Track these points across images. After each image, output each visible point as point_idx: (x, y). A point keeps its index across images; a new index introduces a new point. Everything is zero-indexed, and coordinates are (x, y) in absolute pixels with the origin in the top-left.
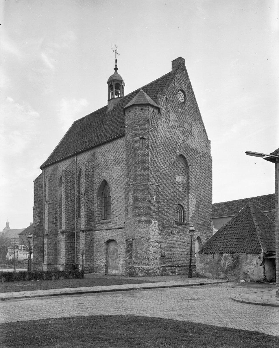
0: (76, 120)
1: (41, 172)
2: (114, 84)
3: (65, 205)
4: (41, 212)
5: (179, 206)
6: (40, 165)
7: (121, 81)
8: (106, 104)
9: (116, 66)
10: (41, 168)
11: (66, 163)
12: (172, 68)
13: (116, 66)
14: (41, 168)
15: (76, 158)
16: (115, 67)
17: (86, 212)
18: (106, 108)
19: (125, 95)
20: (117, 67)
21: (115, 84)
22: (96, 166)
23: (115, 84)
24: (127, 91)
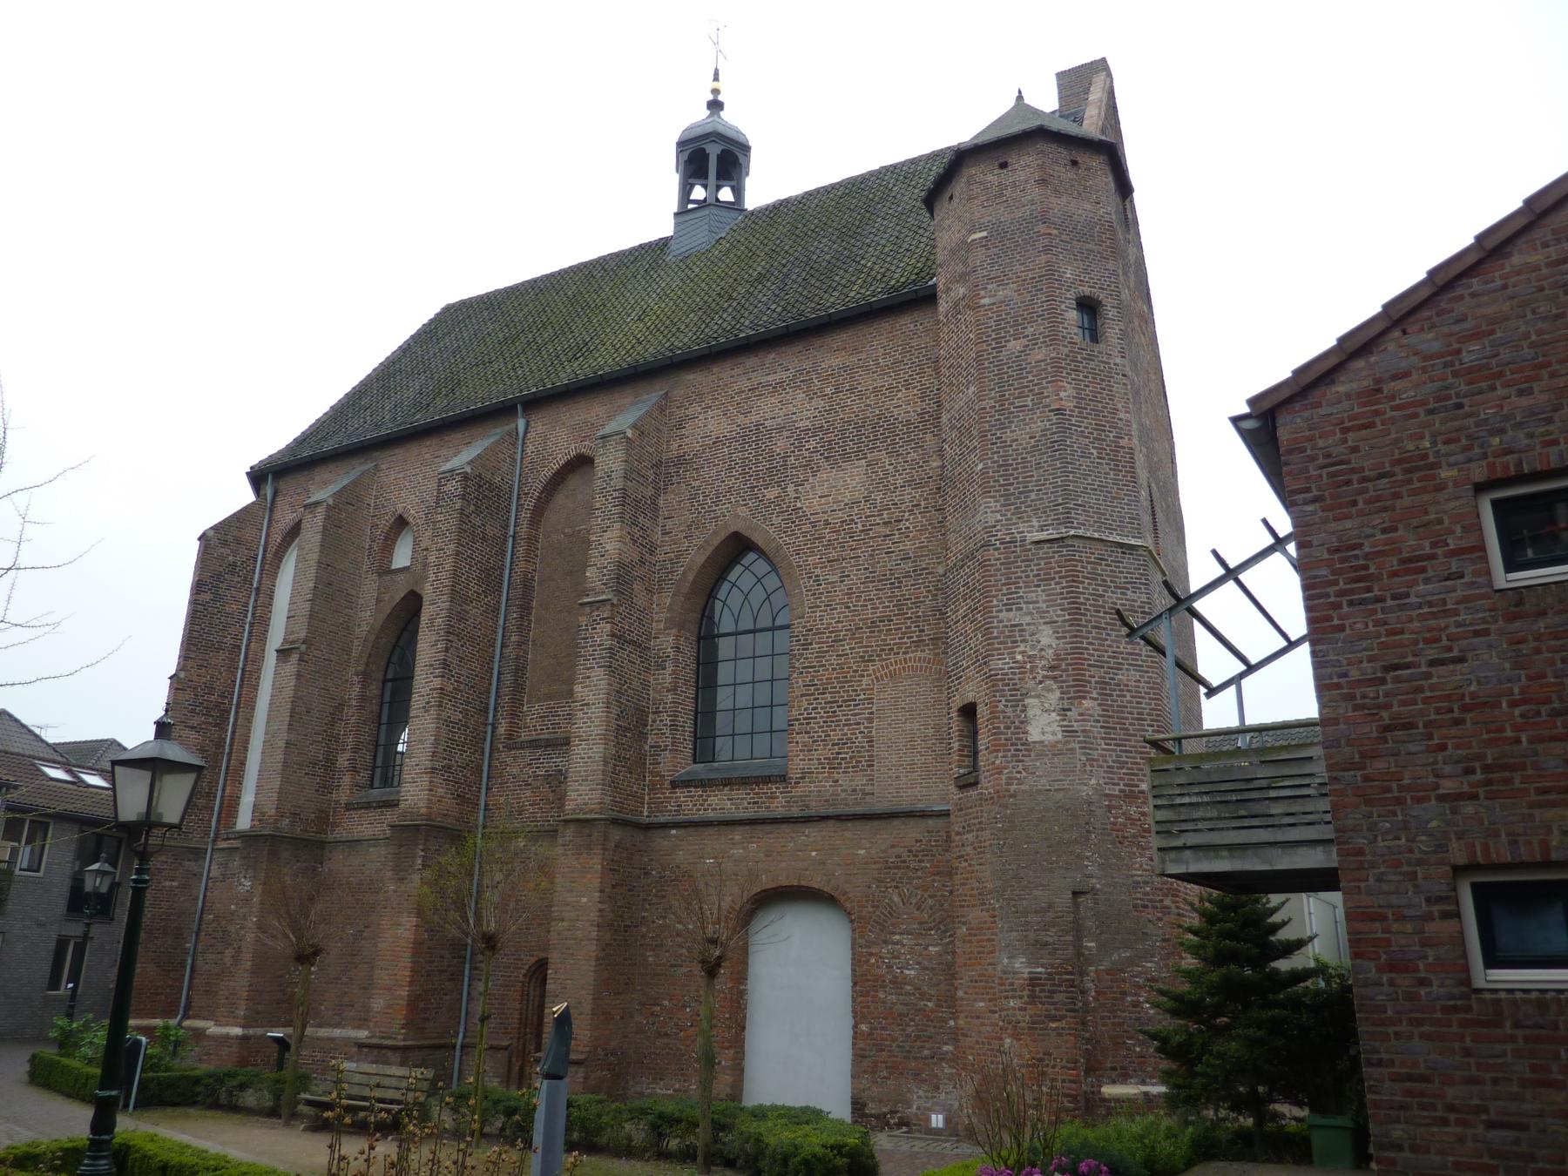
0: (454, 298)
1: (247, 496)
2: (713, 151)
3: (445, 664)
4: (218, 705)
5: (645, 815)
6: (255, 462)
7: (746, 149)
8: (661, 225)
9: (716, 92)
10: (258, 477)
11: (498, 430)
12: (1060, 98)
13: (716, 92)
14: (258, 477)
15: (527, 425)
16: (711, 97)
17: (615, 710)
18: (663, 243)
19: (752, 201)
20: (720, 98)
21: (712, 157)
22: (681, 461)
23: (712, 157)
24: (763, 187)
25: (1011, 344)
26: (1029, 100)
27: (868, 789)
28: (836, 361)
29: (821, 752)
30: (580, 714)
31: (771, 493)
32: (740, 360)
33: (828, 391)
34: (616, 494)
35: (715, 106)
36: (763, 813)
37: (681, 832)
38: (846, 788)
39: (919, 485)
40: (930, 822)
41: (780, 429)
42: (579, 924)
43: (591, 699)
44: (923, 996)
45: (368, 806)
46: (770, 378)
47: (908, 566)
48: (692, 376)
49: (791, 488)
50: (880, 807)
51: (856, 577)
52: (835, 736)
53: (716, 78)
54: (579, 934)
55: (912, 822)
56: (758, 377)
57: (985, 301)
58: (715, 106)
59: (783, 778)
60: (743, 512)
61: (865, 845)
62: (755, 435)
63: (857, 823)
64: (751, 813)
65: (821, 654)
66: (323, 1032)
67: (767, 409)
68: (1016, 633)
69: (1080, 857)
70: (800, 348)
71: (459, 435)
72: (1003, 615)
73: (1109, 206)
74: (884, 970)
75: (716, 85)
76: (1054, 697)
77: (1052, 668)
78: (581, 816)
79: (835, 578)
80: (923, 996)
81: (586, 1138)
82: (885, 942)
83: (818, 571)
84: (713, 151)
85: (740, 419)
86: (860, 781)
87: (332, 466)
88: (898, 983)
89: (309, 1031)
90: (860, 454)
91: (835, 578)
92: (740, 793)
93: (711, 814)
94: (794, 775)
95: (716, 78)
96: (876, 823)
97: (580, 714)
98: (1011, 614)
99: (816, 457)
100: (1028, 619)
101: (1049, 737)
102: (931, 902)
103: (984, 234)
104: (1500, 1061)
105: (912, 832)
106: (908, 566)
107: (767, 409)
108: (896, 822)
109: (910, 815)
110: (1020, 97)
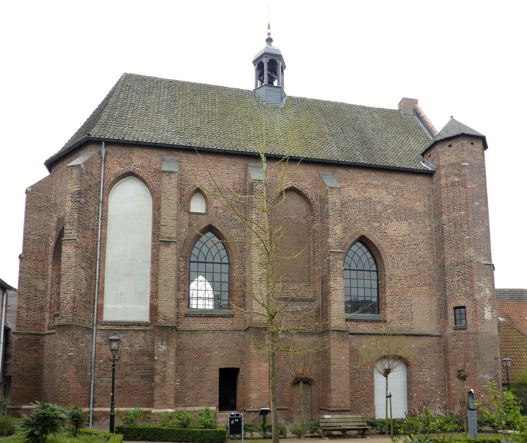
2: (265, 61)
9: (269, 34)
13: (269, 34)
16: (267, 37)
20: (271, 37)
25: (476, 203)
26: (454, 118)
27: (411, 327)
28: (397, 184)
29: (396, 314)
30: (334, 293)
31: (376, 225)
32: (361, 171)
33: (394, 193)
34: (338, 212)
35: (269, 40)
36: (378, 332)
37: (353, 336)
38: (405, 326)
39: (424, 235)
40: (433, 338)
41: (379, 202)
42: (342, 366)
43: (338, 287)
44: (431, 386)
45: (222, 316)
46: (373, 182)
47: (421, 260)
48: (341, 171)
49: (383, 225)
50: (415, 332)
51: (406, 260)
52: (401, 310)
53: (269, 28)
54: (342, 369)
55: (428, 338)
56: (368, 180)
57: (468, 186)
58: (269, 40)
59: (385, 321)
60: (366, 229)
61: (415, 343)
62: (368, 201)
63: (412, 337)
64: (374, 332)
65: (395, 283)
66: (121, 409)
67: (372, 193)
68: (480, 289)
69: (496, 350)
70: (383, 174)
71: (228, 160)
72: (477, 283)
73: (117, 93)
74: (420, 379)
75: (269, 31)
76: (490, 307)
77: (489, 300)
78: (338, 329)
79: (399, 259)
80: (431, 386)
81: (299, 435)
82: (421, 371)
83: (394, 256)
84: (265, 61)
85: (362, 194)
86: (409, 324)
87: (146, 150)
88: (424, 382)
89: (115, 409)
90: (406, 219)
91: (399, 259)
92: (370, 325)
93: (360, 331)
94: (388, 321)
95: (269, 28)
96: (417, 337)
97: (334, 293)
98: (479, 283)
99: (391, 216)
100: (483, 285)
101: (489, 318)
102: (433, 360)
103: (468, 164)
104: (91, 404)
105: (428, 340)
106: (421, 260)
107: (372, 193)
108: (424, 337)
109: (428, 335)
110: (452, 117)
